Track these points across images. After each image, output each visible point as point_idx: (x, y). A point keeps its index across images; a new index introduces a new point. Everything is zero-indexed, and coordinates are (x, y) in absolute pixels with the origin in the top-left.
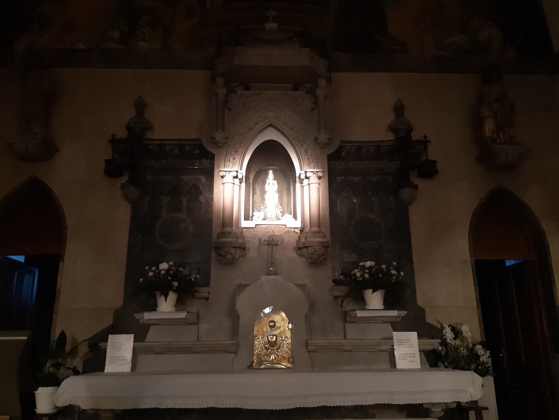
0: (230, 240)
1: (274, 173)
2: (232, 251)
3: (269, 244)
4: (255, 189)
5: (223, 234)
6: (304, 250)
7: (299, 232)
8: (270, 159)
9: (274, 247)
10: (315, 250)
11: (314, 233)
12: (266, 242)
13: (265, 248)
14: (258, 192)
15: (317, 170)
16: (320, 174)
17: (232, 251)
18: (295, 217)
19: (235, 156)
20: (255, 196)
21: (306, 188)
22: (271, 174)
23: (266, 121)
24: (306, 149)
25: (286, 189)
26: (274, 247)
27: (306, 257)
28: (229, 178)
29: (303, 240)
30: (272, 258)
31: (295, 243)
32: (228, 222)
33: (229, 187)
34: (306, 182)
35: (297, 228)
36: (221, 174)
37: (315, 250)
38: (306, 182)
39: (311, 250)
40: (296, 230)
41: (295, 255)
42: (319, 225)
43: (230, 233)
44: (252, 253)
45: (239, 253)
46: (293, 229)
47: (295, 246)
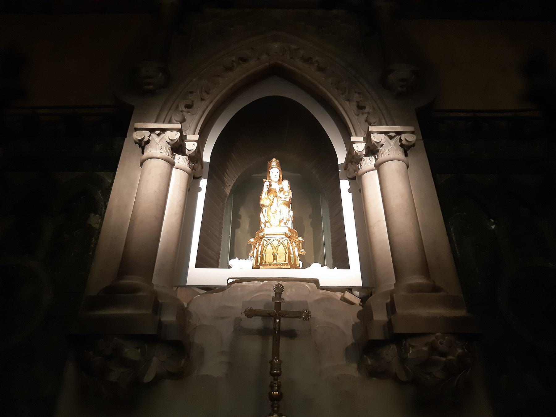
0: (128, 311)
1: (283, 167)
2: (131, 352)
3: (263, 333)
4: (240, 217)
5: (114, 294)
6: (390, 353)
7: (357, 301)
8: (271, 132)
9: (283, 342)
10: (433, 348)
11: (414, 289)
12: (257, 323)
13: (253, 347)
14: (245, 223)
15: (399, 128)
16: (411, 138)
17: (131, 352)
18: (341, 262)
19: (188, 116)
20: (238, 232)
21: (371, 182)
22: (275, 172)
23: (264, 57)
24: (358, 102)
25: (310, 217)
26: (283, 342)
27: (395, 378)
28: (158, 148)
29: (380, 316)
30: (276, 376)
31: (349, 332)
32: (142, 263)
33: (158, 177)
34: (369, 162)
35: (350, 289)
36: (137, 135)
37: (433, 348)
38: (369, 162)
39: (417, 350)
40: (348, 295)
41: (352, 370)
42: (425, 268)
43: (134, 289)
44: (213, 366)
45: (158, 362)
46: (339, 295)
47: (350, 340)
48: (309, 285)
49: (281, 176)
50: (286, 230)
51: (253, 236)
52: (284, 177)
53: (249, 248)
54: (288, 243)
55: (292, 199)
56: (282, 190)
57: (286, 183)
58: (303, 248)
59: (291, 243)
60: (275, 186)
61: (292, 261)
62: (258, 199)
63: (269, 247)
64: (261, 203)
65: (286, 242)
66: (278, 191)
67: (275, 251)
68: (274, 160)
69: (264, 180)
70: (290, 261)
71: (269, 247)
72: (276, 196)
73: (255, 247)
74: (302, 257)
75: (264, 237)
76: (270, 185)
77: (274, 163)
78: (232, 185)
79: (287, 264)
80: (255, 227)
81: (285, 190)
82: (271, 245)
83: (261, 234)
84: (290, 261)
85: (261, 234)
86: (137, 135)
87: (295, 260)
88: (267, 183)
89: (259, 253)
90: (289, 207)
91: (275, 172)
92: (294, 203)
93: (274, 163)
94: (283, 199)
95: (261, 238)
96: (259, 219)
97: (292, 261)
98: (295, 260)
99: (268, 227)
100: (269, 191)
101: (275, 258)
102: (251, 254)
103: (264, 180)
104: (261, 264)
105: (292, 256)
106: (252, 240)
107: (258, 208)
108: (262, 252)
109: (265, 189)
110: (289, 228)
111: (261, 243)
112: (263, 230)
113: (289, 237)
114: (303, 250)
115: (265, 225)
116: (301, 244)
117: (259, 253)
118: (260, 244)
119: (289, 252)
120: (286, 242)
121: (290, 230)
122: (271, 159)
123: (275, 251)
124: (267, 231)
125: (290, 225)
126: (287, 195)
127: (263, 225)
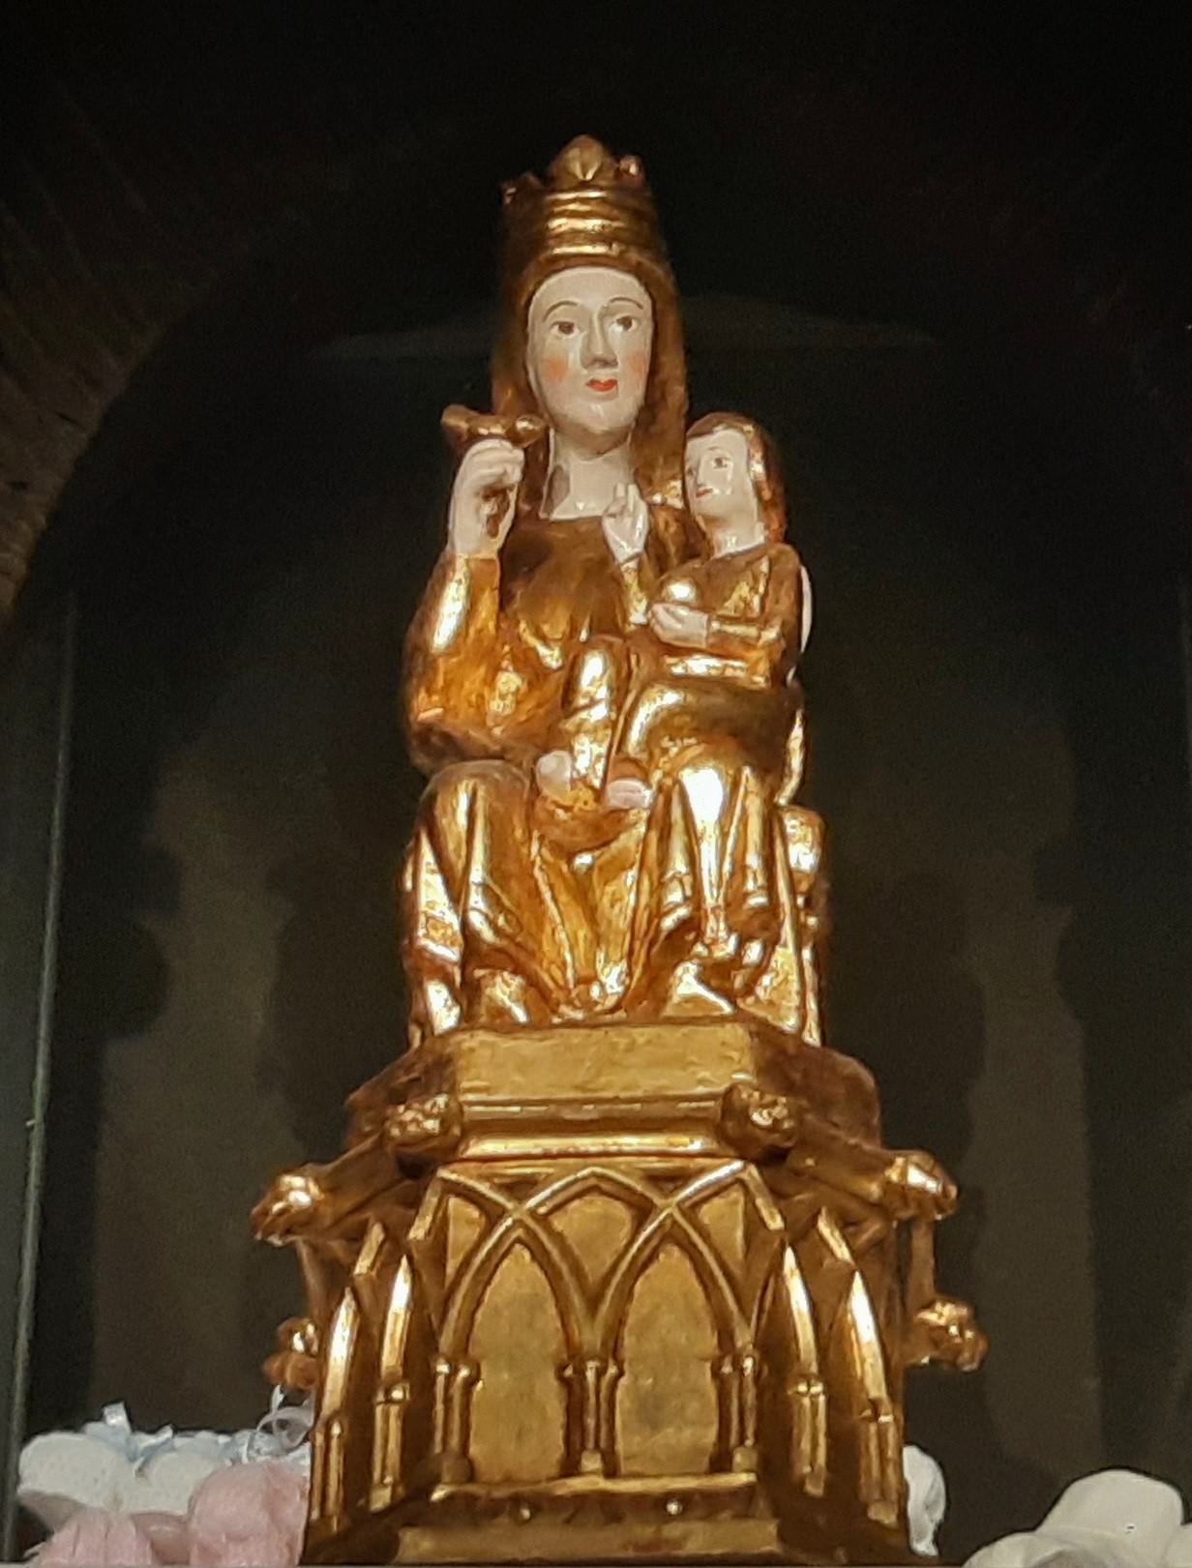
1: (684, 245)
14: (227, 959)
20: (129, 1062)
22: (591, 316)
48: (486, 620)
49: (674, 366)
50: (721, 1065)
51: (316, 1146)
52: (704, 372)
53: (276, 1289)
54: (754, 1223)
55: (816, 674)
56: (681, 545)
57: (728, 464)
58: (948, 1288)
59: (801, 1235)
60: (598, 497)
61: (811, 1452)
62: (390, 651)
63: (518, 1275)
64: (426, 709)
65: (724, 1218)
66: (627, 542)
67: (590, 1336)
68: (583, 159)
69: (456, 419)
70: (775, 1460)
71: (518, 1275)
72: (608, 624)
73: (338, 1277)
74: (933, 1404)
75: (449, 1153)
76: (541, 473)
77: (583, 206)
78: (50, 482)
79: (742, 1501)
80: (350, 1024)
81: (730, 542)
82: (540, 1256)
83: (419, 1119)
84: (775, 1460)
85: (419, 1119)
86: (606, 901)
87: (844, 1445)
88: (490, 459)
89: (390, 1356)
90: (771, 766)
91: (591, 316)
92: (839, 713)
93: (583, 206)
94: (699, 665)
95: (416, 1168)
96: (396, 914)
97: (811, 1452)
98: (844, 1445)
99: (501, 1022)
100: (528, 558)
101: (583, 1424)
102: (287, 1368)
103: (456, 419)
104: (412, 1506)
105: (810, 1395)
106: (300, 1191)
107: (387, 789)
108: (422, 1339)
109: (471, 534)
110: (765, 1034)
111: (418, 1232)
112: (440, 1071)
113: (771, 1157)
114: (944, 1314)
115: (467, 994)
116: (922, 1243)
117: (390, 1356)
118: (395, 1247)
119: (775, 1343)
120: (724, 1218)
121: (778, 1059)
122: (540, 165)
123: (590, 1336)
124: (496, 1072)
125: (787, 984)
126: (733, 627)
127: (440, 1006)
